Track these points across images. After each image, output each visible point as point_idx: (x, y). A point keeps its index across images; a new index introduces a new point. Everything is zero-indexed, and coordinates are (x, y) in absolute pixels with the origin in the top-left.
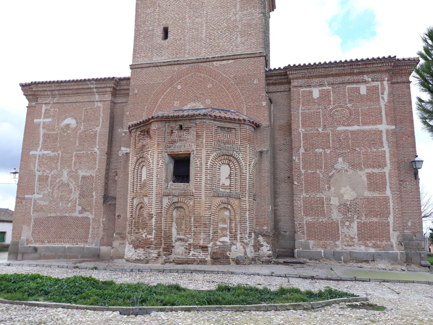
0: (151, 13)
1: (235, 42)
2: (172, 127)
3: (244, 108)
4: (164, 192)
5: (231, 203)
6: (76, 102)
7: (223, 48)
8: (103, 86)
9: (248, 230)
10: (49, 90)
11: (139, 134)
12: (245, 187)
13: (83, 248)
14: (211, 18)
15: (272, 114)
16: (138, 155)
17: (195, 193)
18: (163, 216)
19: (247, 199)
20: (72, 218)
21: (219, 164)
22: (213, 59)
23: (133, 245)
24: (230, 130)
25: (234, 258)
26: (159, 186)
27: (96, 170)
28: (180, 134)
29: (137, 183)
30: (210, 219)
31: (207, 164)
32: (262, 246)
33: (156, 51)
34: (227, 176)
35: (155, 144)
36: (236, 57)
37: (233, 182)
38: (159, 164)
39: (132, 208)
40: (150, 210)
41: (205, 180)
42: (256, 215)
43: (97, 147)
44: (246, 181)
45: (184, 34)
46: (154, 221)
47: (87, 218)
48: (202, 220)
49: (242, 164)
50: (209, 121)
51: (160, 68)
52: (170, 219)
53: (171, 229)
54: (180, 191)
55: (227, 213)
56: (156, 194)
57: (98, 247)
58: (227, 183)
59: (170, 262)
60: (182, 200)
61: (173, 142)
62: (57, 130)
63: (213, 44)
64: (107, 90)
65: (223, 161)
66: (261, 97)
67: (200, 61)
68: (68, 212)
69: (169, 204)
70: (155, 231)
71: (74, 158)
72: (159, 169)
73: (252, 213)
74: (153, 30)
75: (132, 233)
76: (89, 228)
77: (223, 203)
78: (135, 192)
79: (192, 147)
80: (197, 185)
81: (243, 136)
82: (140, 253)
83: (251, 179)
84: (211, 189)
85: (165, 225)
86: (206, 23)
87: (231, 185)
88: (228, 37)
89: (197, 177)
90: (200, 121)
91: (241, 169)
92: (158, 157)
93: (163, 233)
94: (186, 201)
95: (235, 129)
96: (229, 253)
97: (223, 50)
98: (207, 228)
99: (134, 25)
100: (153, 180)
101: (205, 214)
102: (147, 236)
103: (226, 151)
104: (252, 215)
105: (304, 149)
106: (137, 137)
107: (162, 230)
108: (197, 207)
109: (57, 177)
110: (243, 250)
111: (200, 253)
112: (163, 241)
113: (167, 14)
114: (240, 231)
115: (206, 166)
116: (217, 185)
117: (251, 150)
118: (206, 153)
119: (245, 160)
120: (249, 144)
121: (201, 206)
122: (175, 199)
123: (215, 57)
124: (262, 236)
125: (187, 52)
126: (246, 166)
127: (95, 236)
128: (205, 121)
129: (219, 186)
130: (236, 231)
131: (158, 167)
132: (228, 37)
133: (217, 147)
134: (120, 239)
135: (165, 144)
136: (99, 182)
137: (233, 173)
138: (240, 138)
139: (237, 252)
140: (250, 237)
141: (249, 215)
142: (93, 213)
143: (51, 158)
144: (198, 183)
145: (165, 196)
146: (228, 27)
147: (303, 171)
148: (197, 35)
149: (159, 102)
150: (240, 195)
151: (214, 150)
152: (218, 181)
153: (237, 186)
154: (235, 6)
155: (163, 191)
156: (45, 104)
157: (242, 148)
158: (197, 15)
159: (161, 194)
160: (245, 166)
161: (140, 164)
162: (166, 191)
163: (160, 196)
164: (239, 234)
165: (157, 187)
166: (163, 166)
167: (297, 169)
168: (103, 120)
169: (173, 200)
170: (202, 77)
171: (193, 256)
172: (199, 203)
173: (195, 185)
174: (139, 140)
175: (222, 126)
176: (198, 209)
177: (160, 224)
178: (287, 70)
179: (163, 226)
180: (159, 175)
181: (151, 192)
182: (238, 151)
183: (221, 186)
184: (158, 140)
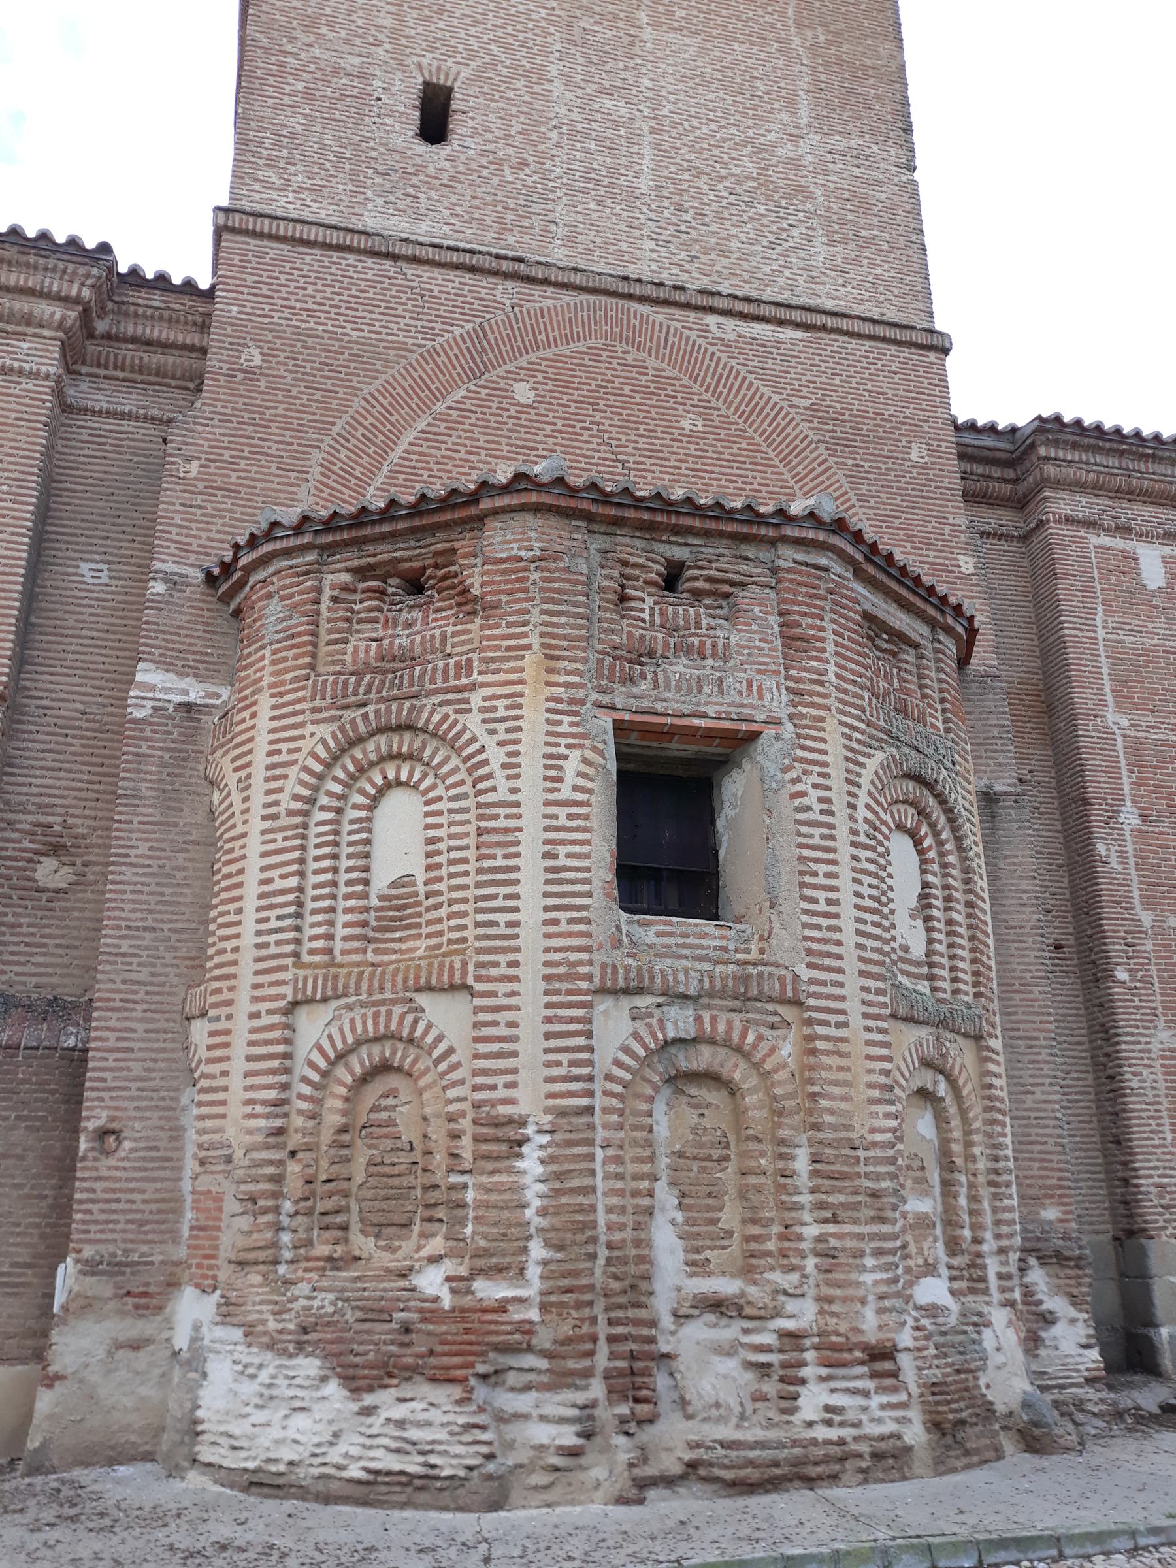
1: (802, 254)
2: (625, 563)
4: (604, 966)
14: (676, 118)
17: (813, 989)
18: (601, 1134)
26: (571, 921)
32: (1048, 1319)
33: (378, 180)
35: (529, 647)
36: (819, 319)
38: (560, 780)
39: (283, 1078)
45: (541, 147)
46: (539, 1170)
51: (410, 270)
54: (706, 967)
56: (547, 978)
59: (668, 1481)
60: (721, 1027)
64: (37, 311)
66: (947, 529)
67: (637, 290)
69: (642, 1053)
72: (562, 812)
75: (276, 1262)
79: (768, 696)
80: (816, 934)
85: (614, 1200)
86: (653, 131)
88: (765, 221)
90: (800, 557)
97: (746, 276)
100: (516, 882)
101: (873, 1131)
105: (1136, 811)
106: (325, 603)
107: (594, 1240)
113: (442, 25)
114: (998, 1237)
121: (847, 1076)
124: (1043, 1260)
128: (824, 562)
132: (765, 221)
145: (615, 992)
147: (1146, 919)
148: (613, 172)
149: (403, 445)
154: (791, 103)
155: (598, 958)
159: (589, 977)
164: (992, 1253)
166: (589, 791)
167: (1119, 903)
169: (661, 1021)
171: (829, 1423)
173: (808, 932)
176: (837, 1091)
179: (601, 1208)
180: (563, 850)
184: (546, 624)
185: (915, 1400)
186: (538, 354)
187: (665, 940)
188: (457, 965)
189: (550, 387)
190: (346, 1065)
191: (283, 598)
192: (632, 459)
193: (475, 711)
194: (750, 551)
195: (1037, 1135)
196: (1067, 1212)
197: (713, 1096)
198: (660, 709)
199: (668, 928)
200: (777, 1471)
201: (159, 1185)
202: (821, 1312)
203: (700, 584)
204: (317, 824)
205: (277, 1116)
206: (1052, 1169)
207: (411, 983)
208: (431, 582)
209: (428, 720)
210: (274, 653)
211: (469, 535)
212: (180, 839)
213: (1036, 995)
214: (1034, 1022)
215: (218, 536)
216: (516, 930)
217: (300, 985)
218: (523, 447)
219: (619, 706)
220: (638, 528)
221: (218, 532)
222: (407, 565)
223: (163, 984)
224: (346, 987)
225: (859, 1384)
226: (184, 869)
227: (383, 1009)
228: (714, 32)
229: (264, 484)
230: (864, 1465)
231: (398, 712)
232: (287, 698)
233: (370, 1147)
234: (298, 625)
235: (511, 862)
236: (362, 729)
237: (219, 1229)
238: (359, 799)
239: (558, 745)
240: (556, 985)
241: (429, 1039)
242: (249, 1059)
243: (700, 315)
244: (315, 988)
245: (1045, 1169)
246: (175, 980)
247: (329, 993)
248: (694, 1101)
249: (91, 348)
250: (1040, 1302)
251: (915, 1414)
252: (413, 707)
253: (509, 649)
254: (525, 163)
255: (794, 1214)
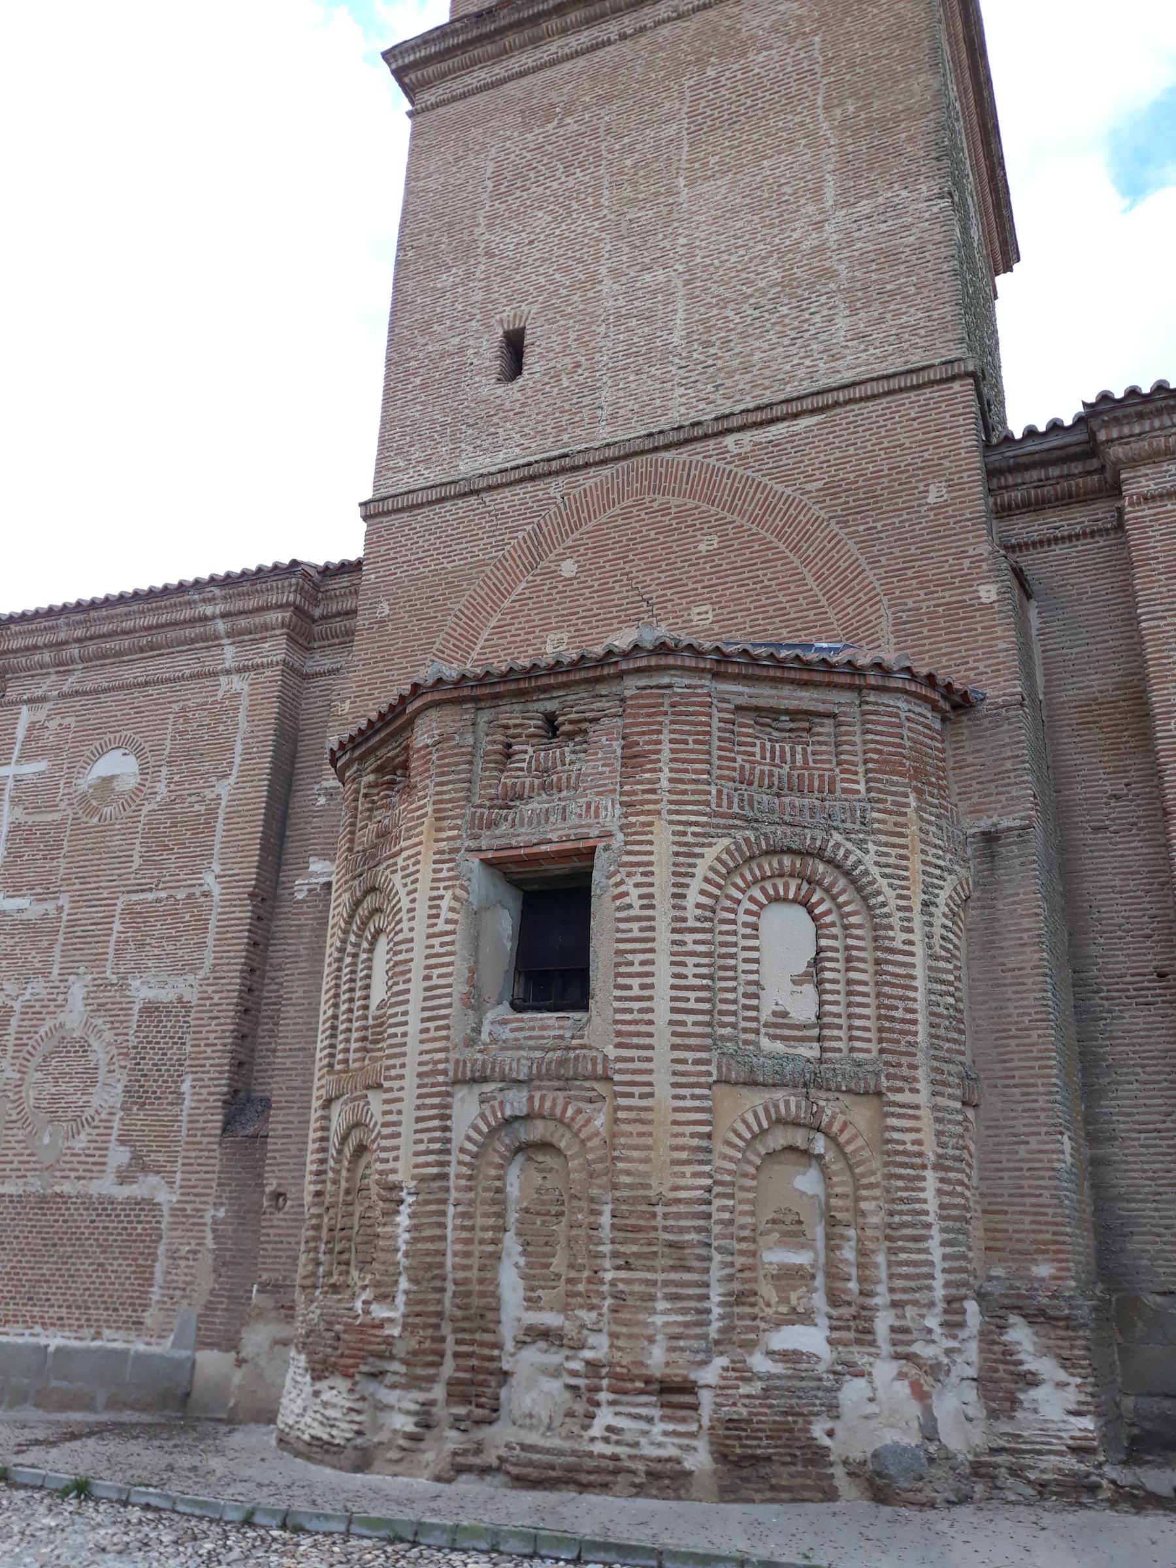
0: (455, 286)
1: (823, 337)
2: (507, 727)
3: (883, 625)
4: (457, 1062)
5: (830, 1124)
6: (147, 684)
7: (767, 372)
8: (252, 603)
9: (938, 1283)
10: (45, 646)
11: (369, 786)
12: (906, 1027)
13: (122, 1355)
14: (708, 261)
15: (1037, 649)
16: (356, 882)
17: (619, 1066)
18: (454, 1195)
19: (923, 1098)
20: (87, 1201)
21: (752, 899)
22: (720, 426)
23: (309, 1354)
24: (806, 725)
25: (857, 1455)
26: (437, 1028)
27: (201, 974)
28: (546, 758)
29: (350, 1021)
30: (708, 1216)
31: (679, 902)
32: (1031, 1380)
33: (470, 431)
34: (802, 968)
36: (830, 398)
37: (837, 1003)
39: (320, 1156)
40: (387, 1161)
41: (673, 987)
42: (983, 1195)
43: (217, 868)
44: (911, 994)
45: (592, 344)
47: (148, 1205)
48: (659, 1222)
49: (881, 899)
50: (687, 682)
51: (486, 497)
52: (486, 1215)
53: (495, 1269)
55: (807, 1182)
57: (184, 1353)
58: (803, 1007)
60: (548, 1105)
61: (510, 799)
62: (63, 805)
63: (720, 363)
65: (775, 886)
66: (966, 563)
67: (661, 441)
68: (73, 1174)
69: (485, 1129)
70: (410, 1280)
71: (117, 926)
72: (436, 941)
73: (961, 1183)
74: (461, 350)
76: (154, 1256)
77: (780, 1122)
78: (338, 1067)
80: (628, 1017)
81: (879, 752)
82: (334, 1406)
83: (943, 982)
84: (709, 1041)
85: (459, 1247)
86: (687, 283)
87: (826, 1020)
88: (787, 321)
89: (630, 975)
90: (643, 682)
91: (876, 928)
92: (434, 880)
93: (449, 1294)
94: (570, 1112)
95: (834, 716)
96: (829, 1425)
97: (767, 382)
98: (689, 1269)
99: (385, 344)
101: (675, 1188)
102: (373, 1307)
103: (788, 830)
104: (962, 1195)
106: (361, 799)
107: (444, 1278)
108: (630, 1141)
109: (44, 1010)
110: (914, 1409)
111: (650, 1420)
112: (450, 1339)
113: (518, 277)
114: (892, 1290)
115: (679, 913)
116: (745, 1019)
117: (929, 823)
118: (675, 843)
119: (897, 875)
120: (919, 792)
121: (650, 1141)
122: (516, 1101)
123: (732, 414)
125: (602, 414)
126: (908, 909)
127: (178, 1293)
128: (666, 680)
129: (754, 1025)
130: (868, 1287)
131: (436, 930)
132: (787, 321)
133: (736, 809)
134: (273, 1314)
135: (468, 811)
136: (213, 1028)
137: (836, 950)
138: (866, 762)
139: (873, 1424)
140: (953, 1325)
141: (940, 1192)
142: (178, 1183)
143: (27, 925)
144: (636, 1005)
146: (787, 284)
148: (650, 338)
150: (877, 1074)
151: (717, 826)
152: (745, 995)
153: (858, 1023)
155: (453, 1056)
156: (30, 701)
157: (875, 815)
158: (647, 260)
160: (900, 909)
161: (364, 924)
162: (470, 1054)
164: (886, 1307)
165: (425, 1036)
166: (455, 922)
168: (246, 751)
169: (501, 1103)
170: (673, 510)
171: (606, 1440)
172: (642, 1122)
173: (618, 1017)
174: (369, 810)
175: (762, 703)
176: (636, 1154)
177: (432, 1239)
178: (1094, 424)
180: (436, 972)
181: (398, 1062)
182: (857, 827)
183: (766, 1025)
184: (437, 793)
185: (705, 1432)
187: (517, 1034)
192: (654, 595)
194: (603, 689)
195: (1030, 1187)
196: (1062, 1269)
197: (549, 1160)
198: (514, 843)
200: (553, 1474)
202: (612, 1346)
206: (1046, 1223)
213: (1034, 1038)
214: (1032, 1068)
220: (515, 696)
225: (643, 1411)
228: (745, 161)
230: (637, 1480)
240: (426, 1080)
245: (1038, 1223)
249: (316, 629)
250: (1021, 1363)
251: (702, 1445)
254: (578, 365)
255: (599, 1261)
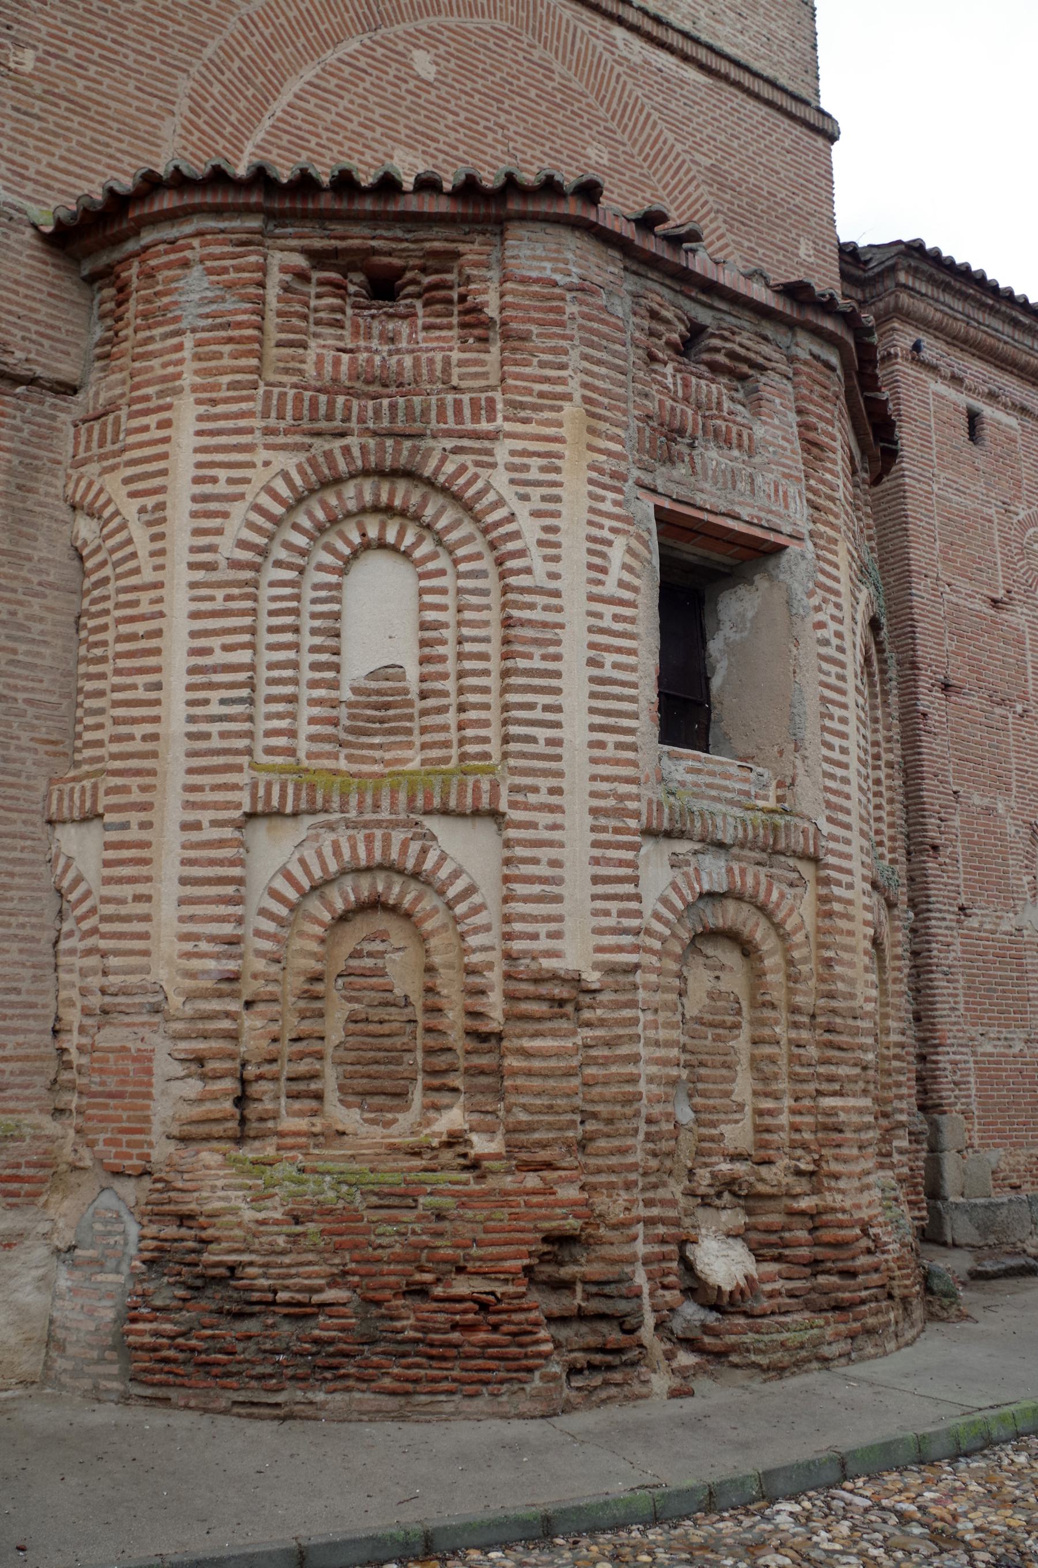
4: (650, 802)
17: (832, 845)
35: (567, 397)
36: (724, 67)
38: (604, 570)
56: (594, 811)
72: (608, 610)
79: (792, 505)
90: (816, 349)
100: (557, 691)
149: (286, 97)
155: (646, 793)
163: (627, 831)
165: (598, 753)
166: (635, 590)
180: (609, 658)
186: (438, 19)
188: (485, 786)
189: (452, 66)
190: (322, 897)
191: (210, 271)
193: (501, 468)
198: (699, 502)
199: (697, 765)
201: (21, 1038)
203: (721, 358)
204: (272, 584)
205: (231, 957)
207: (420, 802)
208: (410, 289)
209: (438, 470)
210: (199, 344)
211: (479, 238)
212: (35, 579)
215: (63, 164)
216: (558, 750)
217: (261, 792)
218: (423, 134)
219: (660, 490)
221: (62, 158)
222: (386, 260)
223: (17, 774)
224: (327, 800)
226: (41, 620)
227: (378, 833)
229: (119, 106)
231: (393, 452)
232: (220, 409)
233: (350, 999)
234: (235, 312)
235: (551, 665)
236: (342, 466)
237: (148, 1096)
238: (328, 559)
239: (601, 527)
240: (603, 821)
241: (443, 874)
242: (184, 881)
243: (607, 23)
244: (283, 796)
246: (34, 769)
247: (303, 806)
248: (709, 962)
252: (415, 450)
253: (541, 395)
